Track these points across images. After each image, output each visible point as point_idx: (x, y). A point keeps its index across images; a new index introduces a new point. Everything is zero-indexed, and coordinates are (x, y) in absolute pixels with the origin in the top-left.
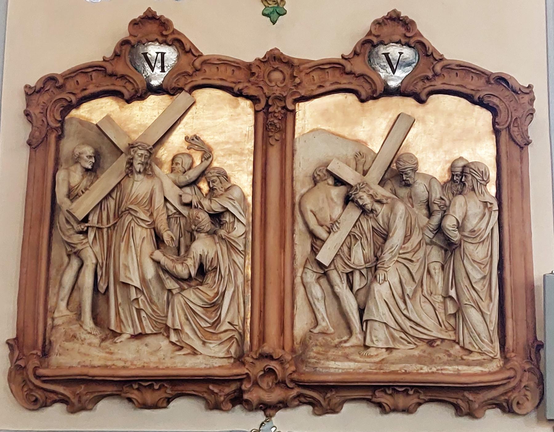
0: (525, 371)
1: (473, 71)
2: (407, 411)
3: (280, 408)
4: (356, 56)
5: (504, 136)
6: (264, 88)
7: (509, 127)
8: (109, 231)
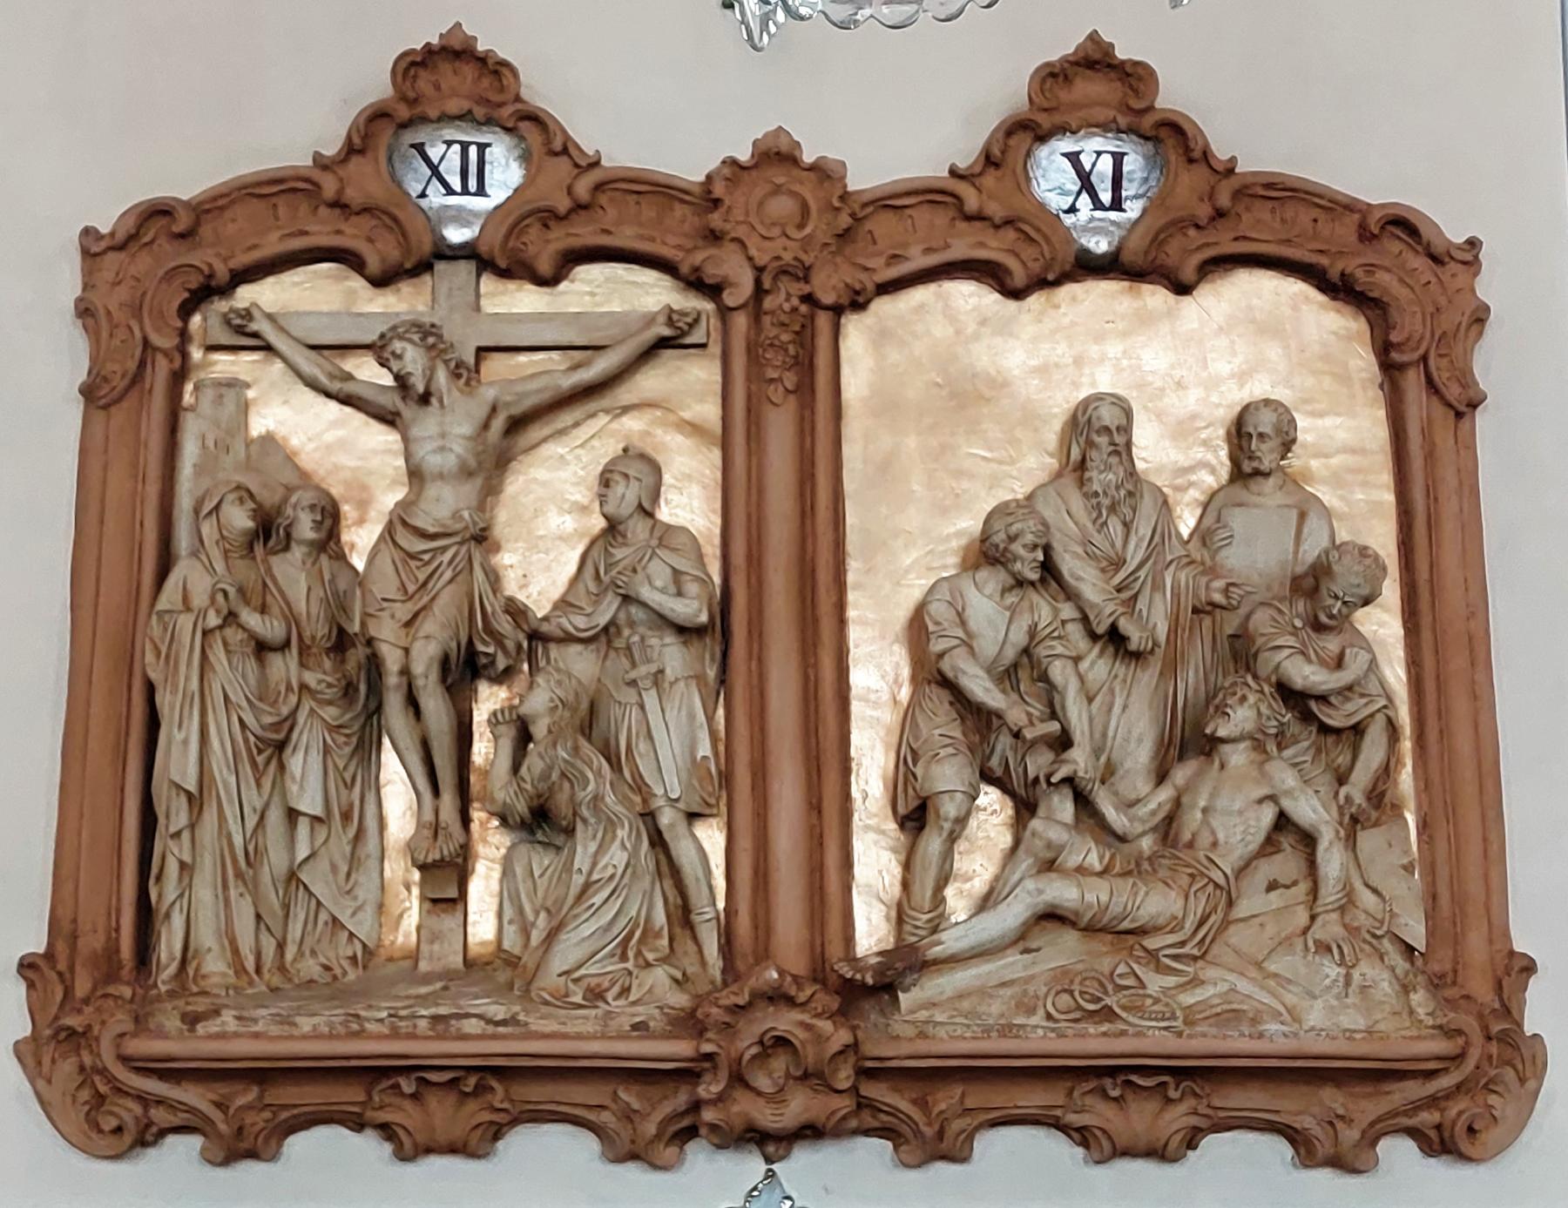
1: (1317, 200)
2: (1159, 1153)
4: (992, 170)
5: (1413, 381)
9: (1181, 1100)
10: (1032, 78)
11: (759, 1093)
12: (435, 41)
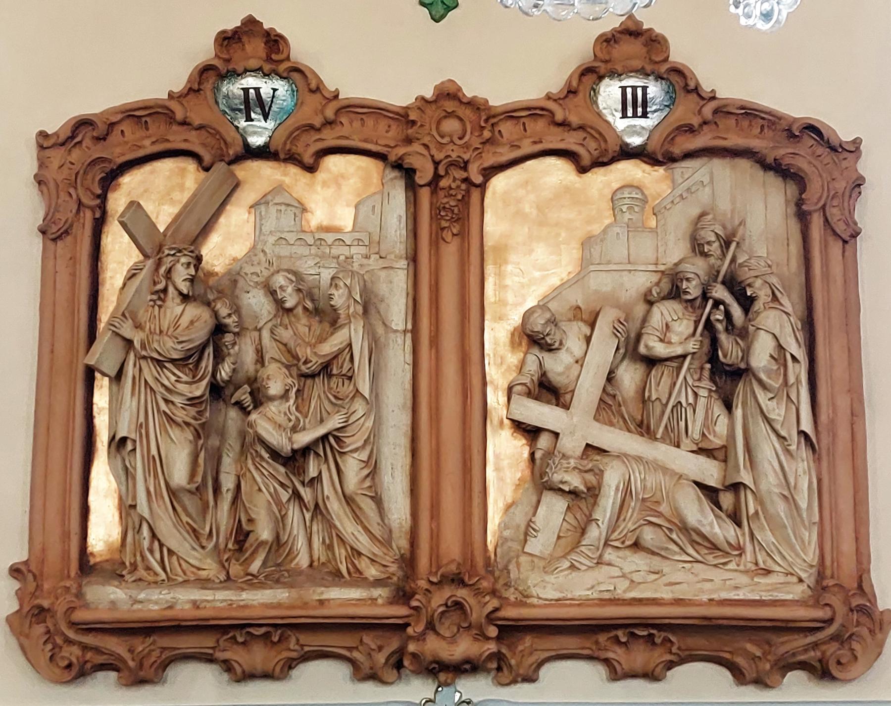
3: (465, 671)
4: (571, 96)
5: (817, 222)
6: (431, 146)
7: (823, 208)
10: (216, 40)
11: (444, 638)
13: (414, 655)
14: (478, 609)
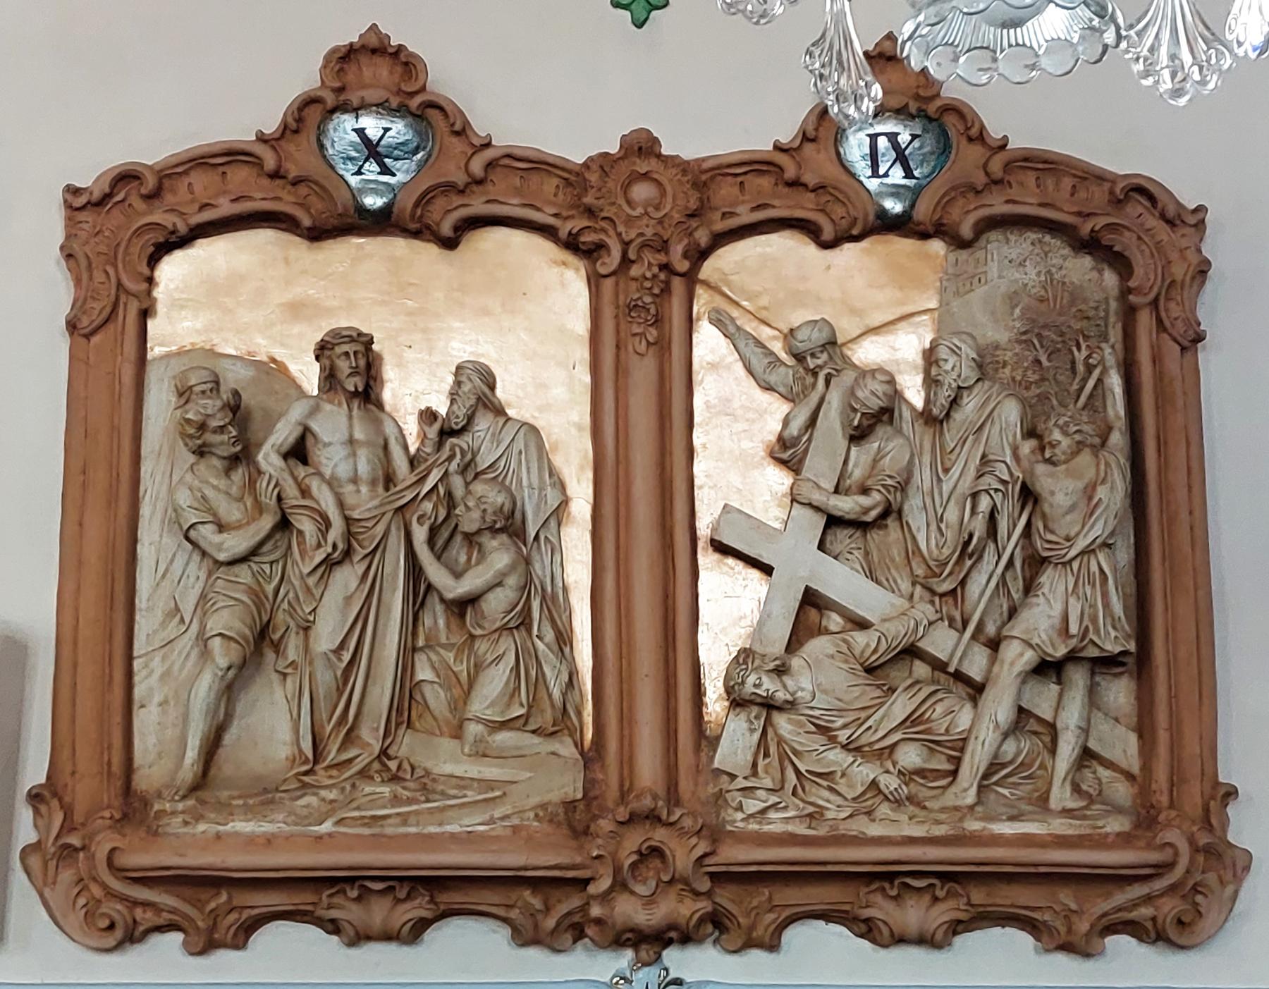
0: (1197, 851)
5: (1145, 320)
7: (1156, 300)
8: (648, 770)
9: (945, 899)
12: (356, 39)
13: (599, 922)
14: (683, 855)
